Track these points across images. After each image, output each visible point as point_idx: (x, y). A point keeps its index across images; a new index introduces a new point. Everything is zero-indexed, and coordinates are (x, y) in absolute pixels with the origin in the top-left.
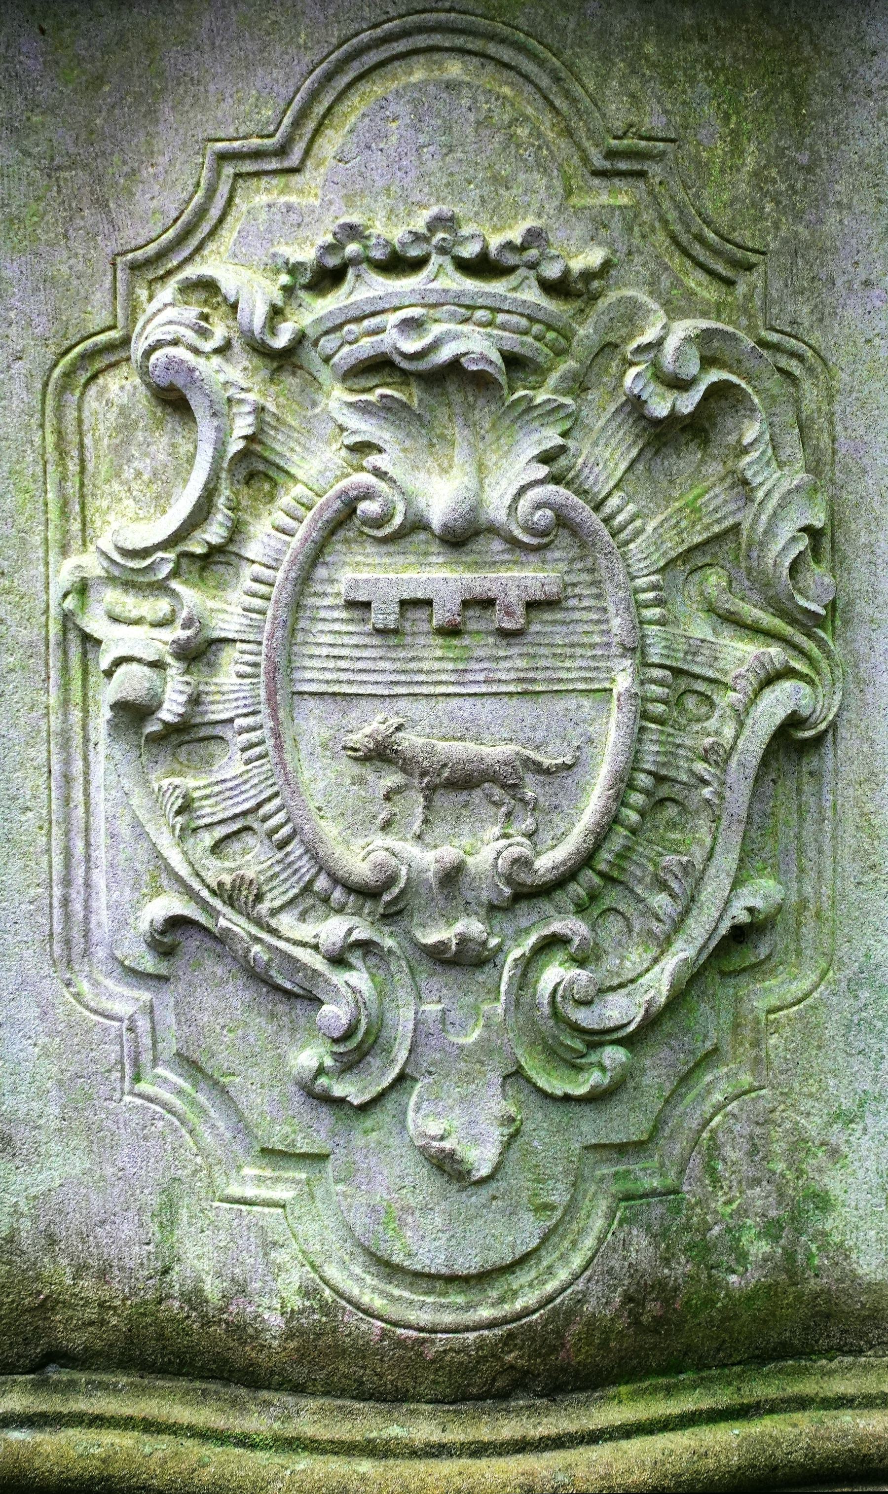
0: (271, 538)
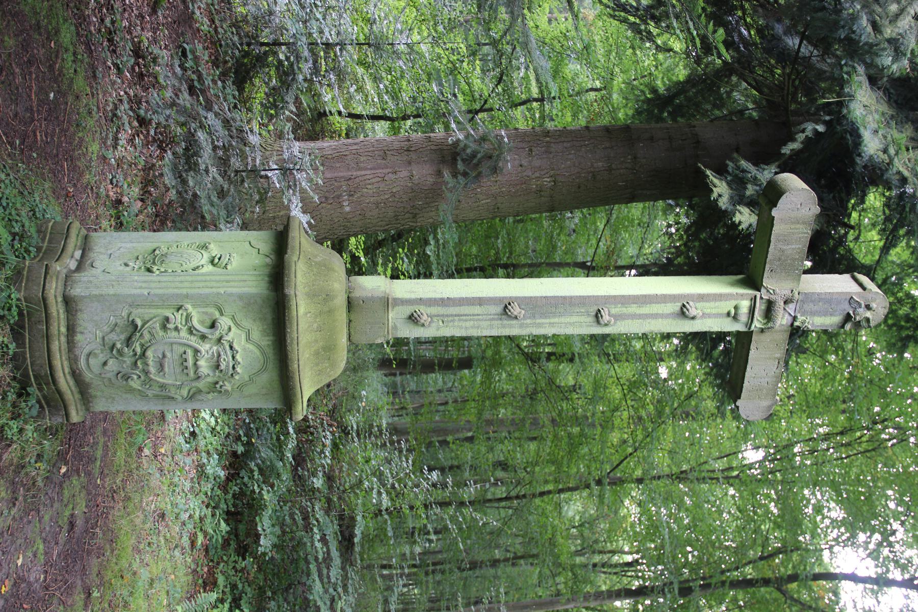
0: (194, 341)
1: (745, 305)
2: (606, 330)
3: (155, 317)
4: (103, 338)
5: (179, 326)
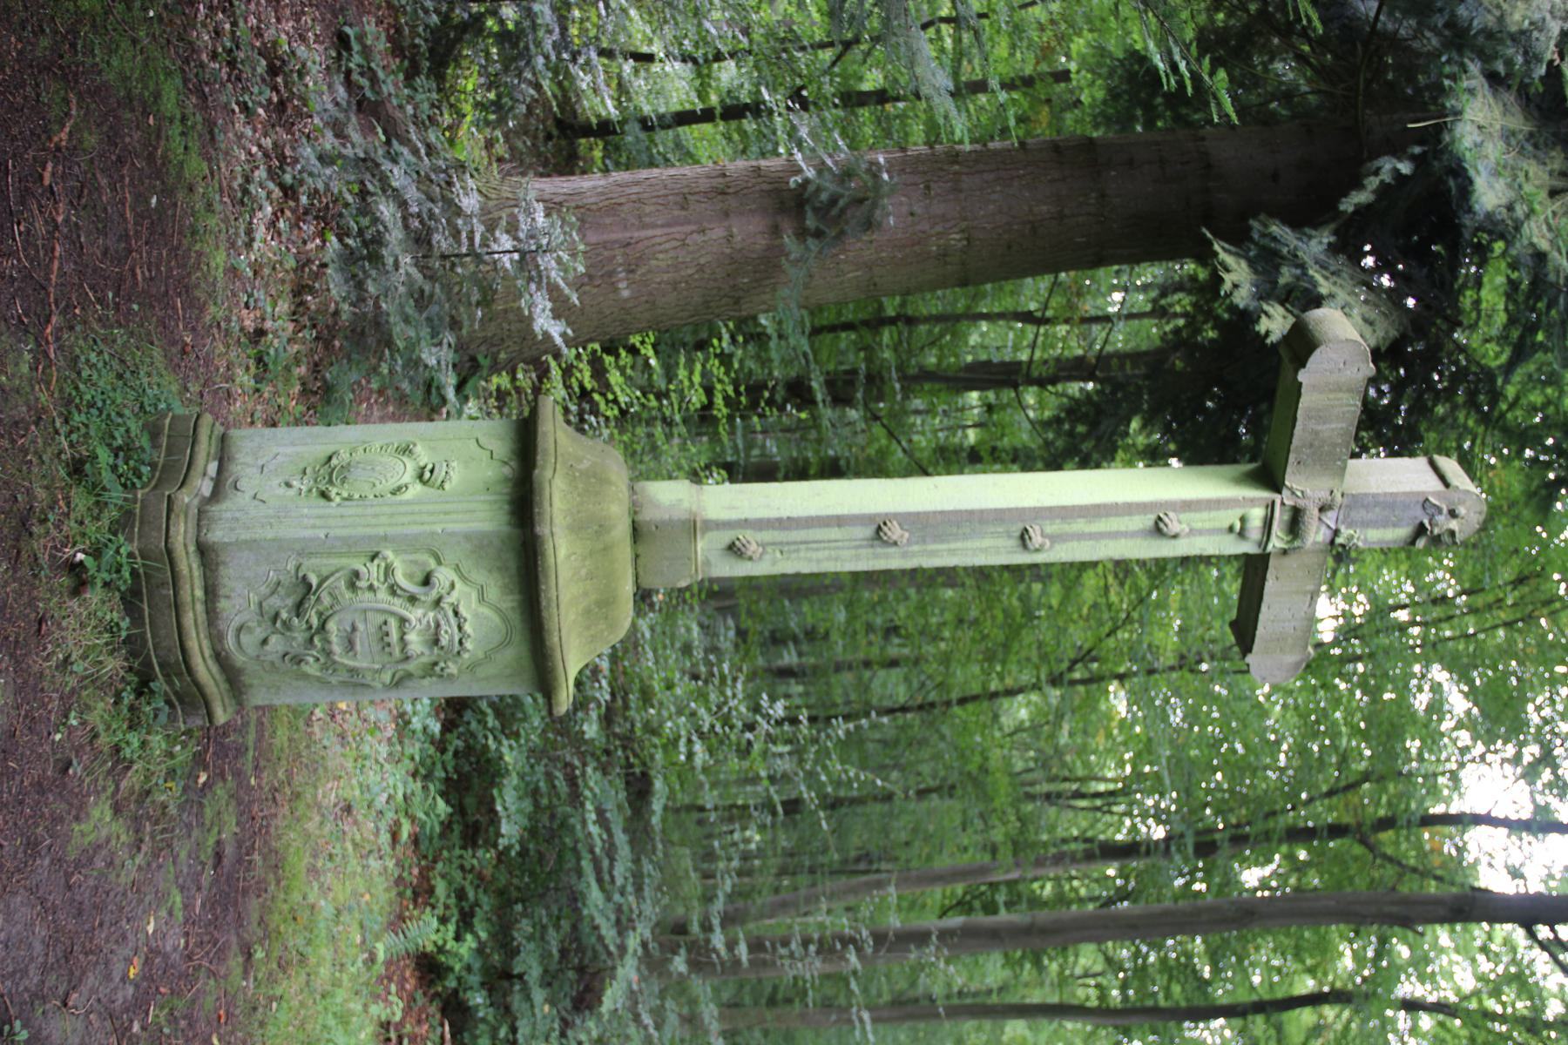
0: (398, 606)
1: (1257, 515)
2: (1039, 558)
3: (337, 571)
4: (260, 604)
5: (376, 584)
